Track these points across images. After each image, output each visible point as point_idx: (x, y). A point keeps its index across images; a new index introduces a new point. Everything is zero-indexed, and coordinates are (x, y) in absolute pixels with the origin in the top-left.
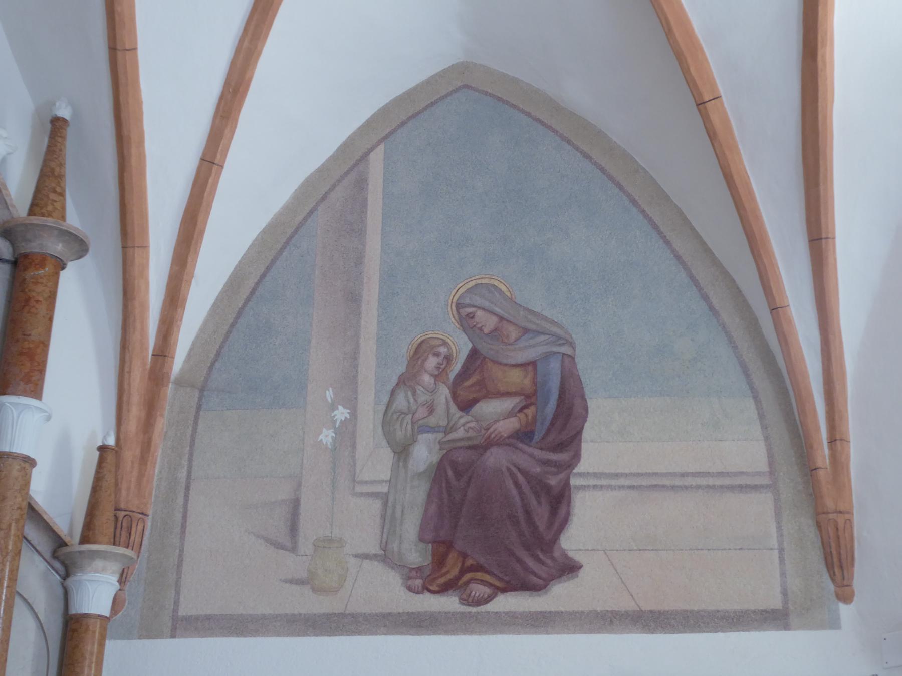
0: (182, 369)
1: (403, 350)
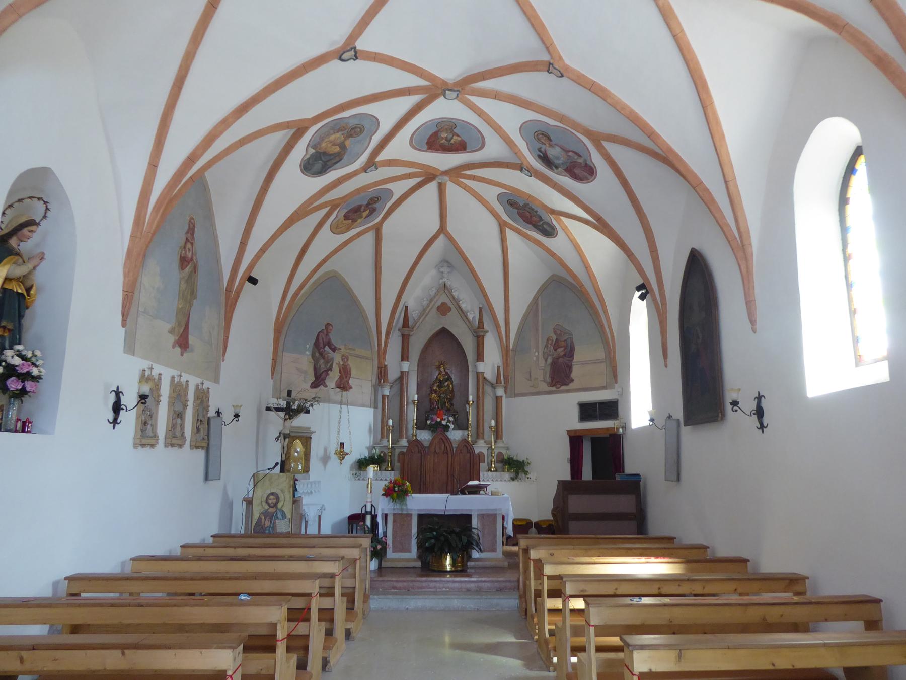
1: (545, 341)
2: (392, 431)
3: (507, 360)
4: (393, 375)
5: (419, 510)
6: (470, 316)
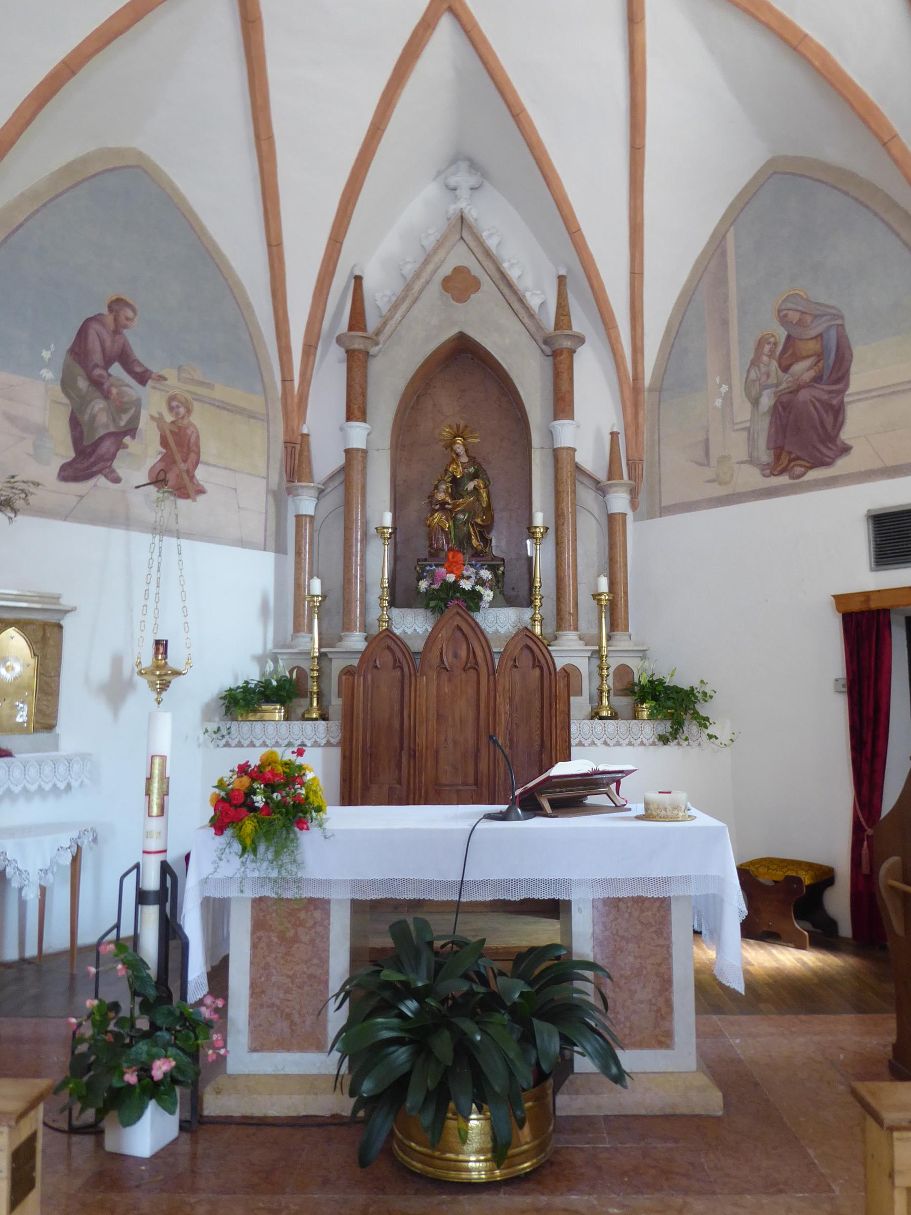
1: (751, 345)
2: (322, 610)
3: (636, 415)
5: (355, 884)
6: (534, 302)
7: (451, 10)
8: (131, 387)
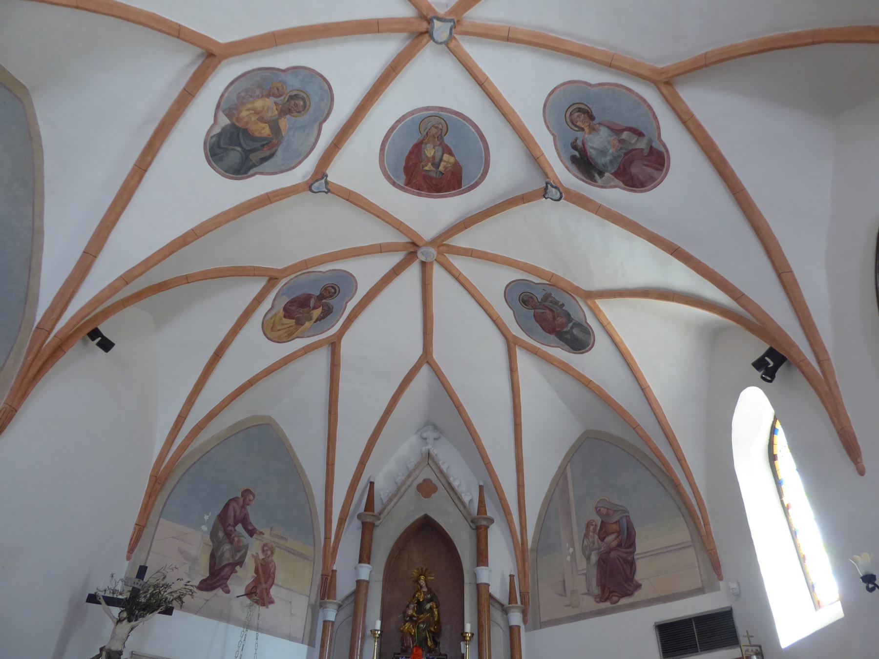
0: (531, 547)
4: (344, 587)
6: (466, 499)
7: (428, 362)
8: (245, 538)
